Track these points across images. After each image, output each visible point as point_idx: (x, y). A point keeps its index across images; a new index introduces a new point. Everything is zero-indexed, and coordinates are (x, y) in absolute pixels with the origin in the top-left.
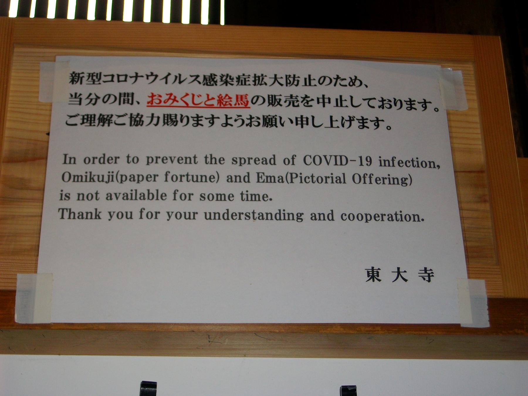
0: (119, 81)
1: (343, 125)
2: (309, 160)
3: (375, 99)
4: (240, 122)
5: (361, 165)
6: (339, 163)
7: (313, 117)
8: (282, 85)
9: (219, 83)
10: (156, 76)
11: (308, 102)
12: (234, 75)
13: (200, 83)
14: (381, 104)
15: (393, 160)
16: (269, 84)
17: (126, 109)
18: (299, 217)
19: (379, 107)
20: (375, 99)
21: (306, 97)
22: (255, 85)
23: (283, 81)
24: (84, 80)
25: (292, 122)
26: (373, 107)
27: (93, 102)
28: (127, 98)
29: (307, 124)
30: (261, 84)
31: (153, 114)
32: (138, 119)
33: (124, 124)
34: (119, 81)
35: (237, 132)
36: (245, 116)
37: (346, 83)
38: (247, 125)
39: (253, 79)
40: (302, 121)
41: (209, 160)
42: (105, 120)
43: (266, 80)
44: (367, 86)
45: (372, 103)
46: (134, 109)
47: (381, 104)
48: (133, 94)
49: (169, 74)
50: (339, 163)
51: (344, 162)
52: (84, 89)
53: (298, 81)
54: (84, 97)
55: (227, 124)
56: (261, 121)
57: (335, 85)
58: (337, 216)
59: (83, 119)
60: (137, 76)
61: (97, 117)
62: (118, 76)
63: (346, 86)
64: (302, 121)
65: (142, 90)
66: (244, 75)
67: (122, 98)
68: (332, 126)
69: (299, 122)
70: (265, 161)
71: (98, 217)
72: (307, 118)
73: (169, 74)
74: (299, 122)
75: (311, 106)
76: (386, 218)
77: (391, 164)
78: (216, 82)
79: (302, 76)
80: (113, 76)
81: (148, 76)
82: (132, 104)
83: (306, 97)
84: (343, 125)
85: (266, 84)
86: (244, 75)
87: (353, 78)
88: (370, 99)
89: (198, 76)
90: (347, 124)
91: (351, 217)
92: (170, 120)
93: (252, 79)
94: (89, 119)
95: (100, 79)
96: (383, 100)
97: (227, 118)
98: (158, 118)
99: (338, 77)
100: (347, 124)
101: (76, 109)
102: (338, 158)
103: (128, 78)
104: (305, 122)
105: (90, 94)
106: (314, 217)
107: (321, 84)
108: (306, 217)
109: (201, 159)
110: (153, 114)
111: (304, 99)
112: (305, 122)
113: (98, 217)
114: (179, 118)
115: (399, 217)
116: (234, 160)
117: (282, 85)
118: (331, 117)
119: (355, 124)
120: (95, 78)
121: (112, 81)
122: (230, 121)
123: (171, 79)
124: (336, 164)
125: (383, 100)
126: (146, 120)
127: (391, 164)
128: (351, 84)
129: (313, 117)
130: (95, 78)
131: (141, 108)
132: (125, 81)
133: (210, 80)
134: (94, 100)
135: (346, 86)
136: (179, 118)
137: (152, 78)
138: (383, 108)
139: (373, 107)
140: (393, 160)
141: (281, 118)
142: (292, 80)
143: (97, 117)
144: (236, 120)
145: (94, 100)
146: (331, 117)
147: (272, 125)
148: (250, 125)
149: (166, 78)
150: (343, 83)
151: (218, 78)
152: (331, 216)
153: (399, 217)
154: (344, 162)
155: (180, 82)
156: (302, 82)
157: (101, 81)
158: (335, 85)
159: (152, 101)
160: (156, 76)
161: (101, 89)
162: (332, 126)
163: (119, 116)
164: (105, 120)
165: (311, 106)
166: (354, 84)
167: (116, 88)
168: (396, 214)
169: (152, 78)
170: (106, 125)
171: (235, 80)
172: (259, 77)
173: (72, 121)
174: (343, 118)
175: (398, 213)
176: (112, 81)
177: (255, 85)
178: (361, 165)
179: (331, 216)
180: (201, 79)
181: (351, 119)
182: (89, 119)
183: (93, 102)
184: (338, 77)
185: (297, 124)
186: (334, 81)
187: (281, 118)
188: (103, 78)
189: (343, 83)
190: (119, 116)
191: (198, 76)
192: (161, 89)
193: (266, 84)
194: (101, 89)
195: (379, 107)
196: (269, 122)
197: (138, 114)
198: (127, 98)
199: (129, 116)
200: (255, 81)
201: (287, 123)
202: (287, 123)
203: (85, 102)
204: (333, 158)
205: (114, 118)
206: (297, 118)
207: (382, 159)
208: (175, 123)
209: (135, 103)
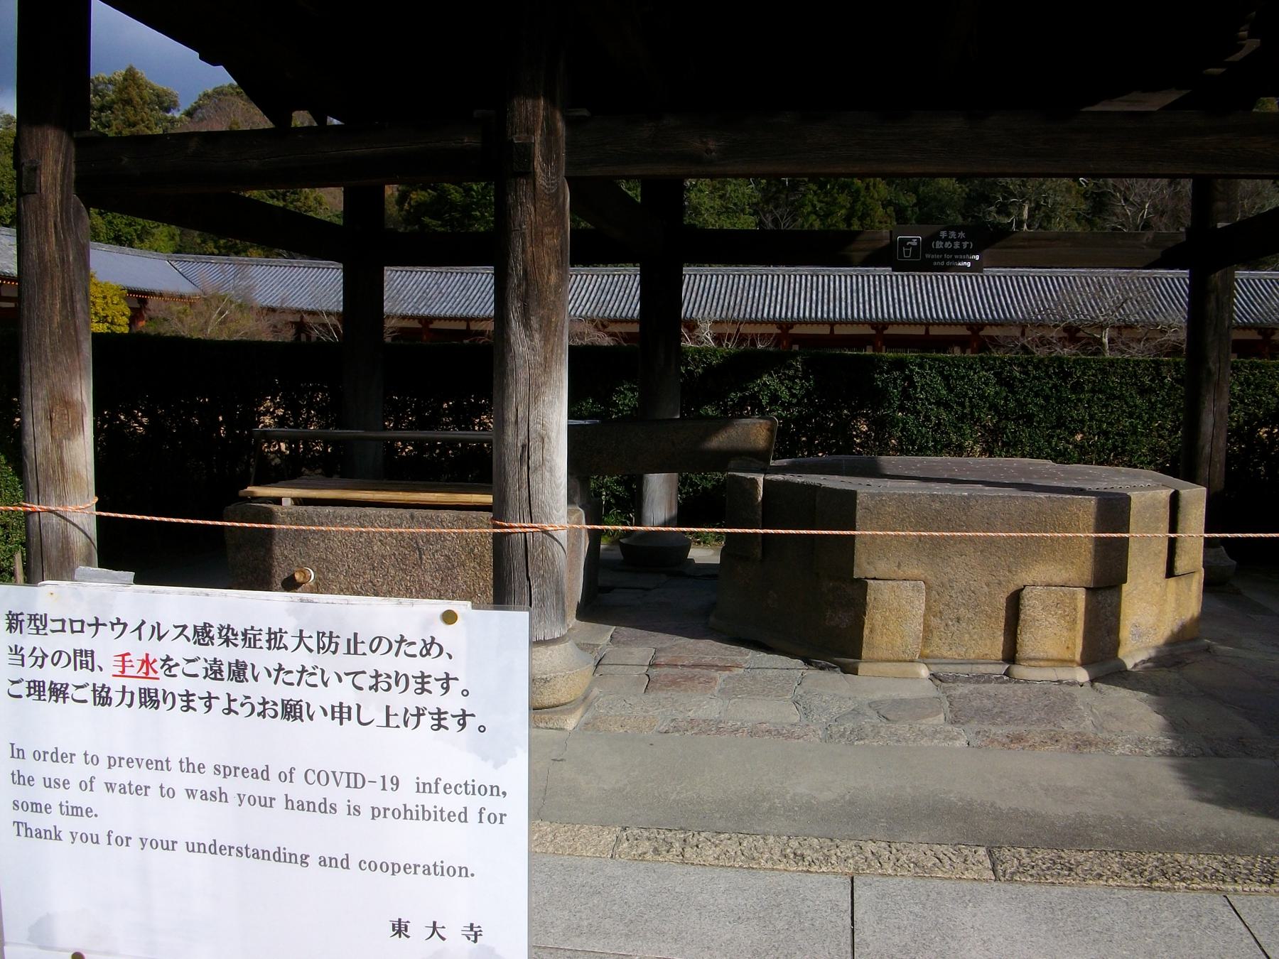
0: (73, 632)
1: (406, 724)
2: (312, 777)
3: (364, 672)
4: (248, 708)
5: (384, 789)
6: (352, 784)
7: (359, 707)
8: (311, 650)
9: (217, 641)
10: (125, 625)
11: (170, 668)
12: (239, 629)
13: (188, 640)
14: (373, 681)
15: (437, 783)
16: (291, 648)
17: (83, 676)
18: (304, 860)
19: (371, 688)
20: (364, 672)
21: (168, 659)
22: (269, 648)
23: (312, 643)
24: (25, 624)
25: (326, 714)
26: (361, 689)
27: (39, 662)
28: (84, 659)
29: (349, 718)
30: (279, 648)
31: (124, 687)
32: (104, 694)
33: (85, 701)
34: (73, 632)
35: (243, 722)
36: (256, 700)
37: (415, 650)
38: (259, 714)
39: (267, 637)
40: (341, 712)
41: (185, 766)
42: (59, 692)
43: (287, 640)
44: (450, 657)
45: (360, 680)
46: (98, 678)
47: (373, 681)
48: (92, 652)
49: (143, 622)
50: (352, 784)
51: (360, 783)
52: (28, 640)
53: (337, 644)
54: (26, 652)
55: (230, 710)
56: (279, 709)
57: (397, 654)
58: (354, 864)
59: (29, 688)
60: (97, 624)
61: (47, 687)
62: (72, 621)
63: (414, 656)
64: (341, 712)
65: (106, 646)
66: (252, 628)
67: (78, 659)
68: (388, 725)
69: (337, 715)
70: (255, 774)
71: (58, 837)
72: (349, 708)
73: (143, 622)
74: (337, 715)
75: (174, 676)
76: (420, 870)
77: (433, 790)
78: (212, 638)
79: (290, 627)
80: (63, 621)
81: (113, 624)
82: (92, 670)
83: (168, 659)
84: (406, 724)
85: (286, 647)
86: (252, 628)
87: (428, 641)
88: (357, 673)
89: (185, 627)
90: (413, 721)
91: (373, 866)
92: (150, 699)
93: (265, 637)
94: (36, 688)
95: (45, 626)
96: (377, 676)
97: (230, 701)
98: (132, 694)
99: (402, 640)
100: (413, 721)
101: (17, 673)
102: (352, 776)
103: (86, 627)
104: (345, 715)
105: (35, 649)
106: (322, 862)
107: (374, 652)
108: (313, 861)
109: (174, 764)
110: (124, 687)
111: (165, 661)
112: (345, 715)
113: (58, 837)
114: (160, 697)
115: (439, 870)
116: (216, 769)
117: (311, 650)
118: (388, 707)
119: (427, 721)
120: (38, 623)
121: (63, 630)
122: (235, 706)
123: (146, 630)
124: (348, 786)
125: (377, 676)
126: (116, 697)
127: (433, 790)
128: (424, 652)
129: (359, 707)
130: (38, 623)
131: (106, 676)
132: (82, 631)
133: (203, 634)
134: (41, 660)
135: (414, 656)
136: (160, 697)
137: (119, 628)
138: (376, 690)
139: (361, 689)
140: (437, 783)
141: (309, 706)
142: (326, 640)
143: (47, 687)
144: (242, 705)
145: (41, 660)
146: (388, 707)
147: (295, 718)
148: (262, 714)
149: (139, 628)
150: (411, 650)
151: (214, 632)
152: (345, 863)
153: (439, 870)
154: (360, 783)
155: (160, 638)
156: (343, 648)
157: (47, 630)
158: (397, 654)
159: (377, 683)
160: (125, 625)
161: (50, 643)
162: (388, 725)
163: (78, 687)
164: (59, 692)
165: (174, 676)
166: (428, 653)
167: (69, 642)
168: (435, 865)
169: (119, 628)
170: (61, 700)
171: (240, 637)
172: (275, 633)
173: (16, 690)
174: (407, 711)
175: (439, 863)
176: (63, 630)
177: (269, 648)
178: (384, 789)
179: (345, 863)
180: (189, 632)
181: (419, 714)
182: (36, 688)
183: (39, 662)
184: (402, 640)
185: (333, 718)
186: (395, 646)
187: (309, 706)
188: (51, 626)
189: (411, 650)
190: (78, 687)
191: (185, 627)
192: (138, 648)
193: (286, 647)
194: (50, 643)
195: (371, 688)
196: (291, 711)
197: (104, 686)
198: (84, 659)
199: (91, 687)
200: (269, 641)
201: (319, 714)
202: (319, 714)
203: (29, 661)
204: (345, 776)
205: (71, 690)
206: (333, 707)
207: (420, 781)
208: (155, 703)
209: (96, 668)
